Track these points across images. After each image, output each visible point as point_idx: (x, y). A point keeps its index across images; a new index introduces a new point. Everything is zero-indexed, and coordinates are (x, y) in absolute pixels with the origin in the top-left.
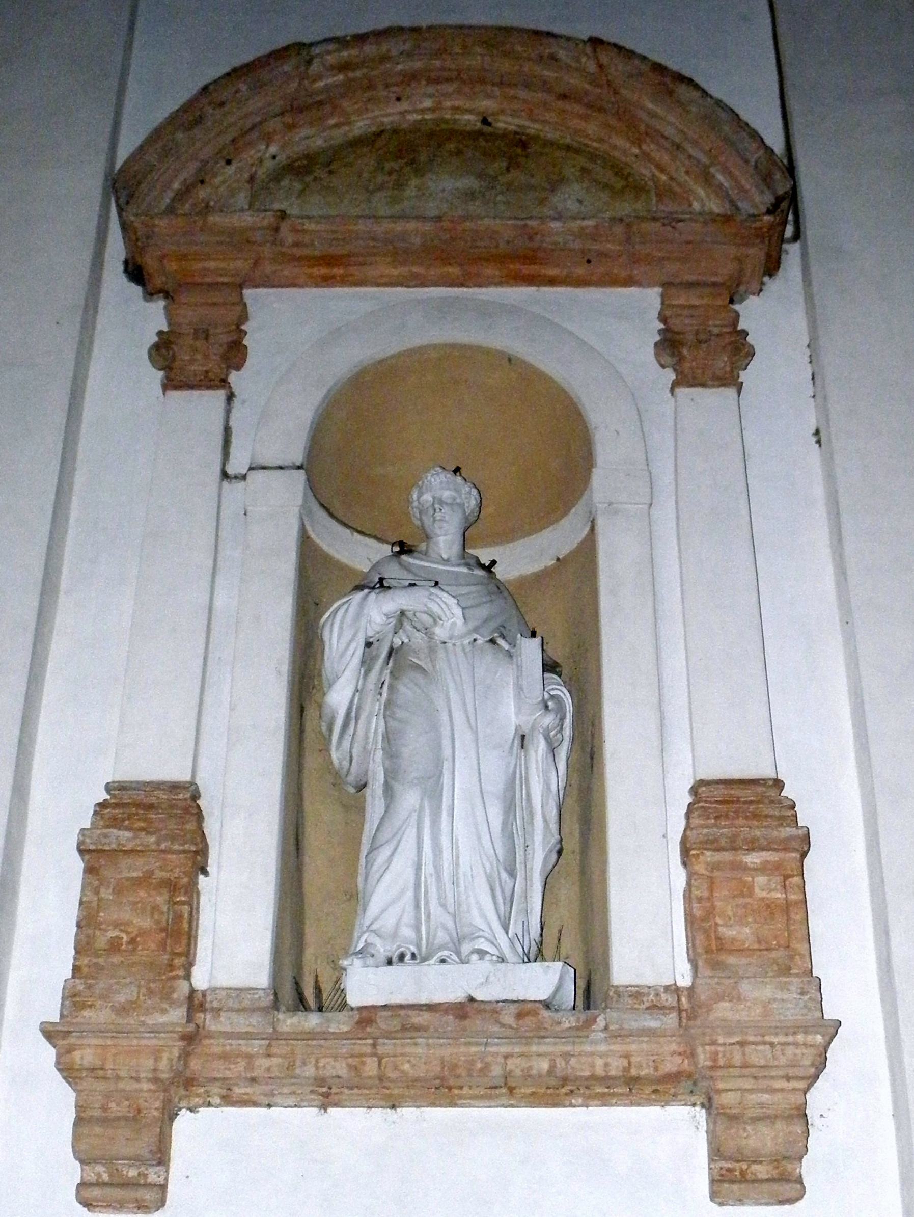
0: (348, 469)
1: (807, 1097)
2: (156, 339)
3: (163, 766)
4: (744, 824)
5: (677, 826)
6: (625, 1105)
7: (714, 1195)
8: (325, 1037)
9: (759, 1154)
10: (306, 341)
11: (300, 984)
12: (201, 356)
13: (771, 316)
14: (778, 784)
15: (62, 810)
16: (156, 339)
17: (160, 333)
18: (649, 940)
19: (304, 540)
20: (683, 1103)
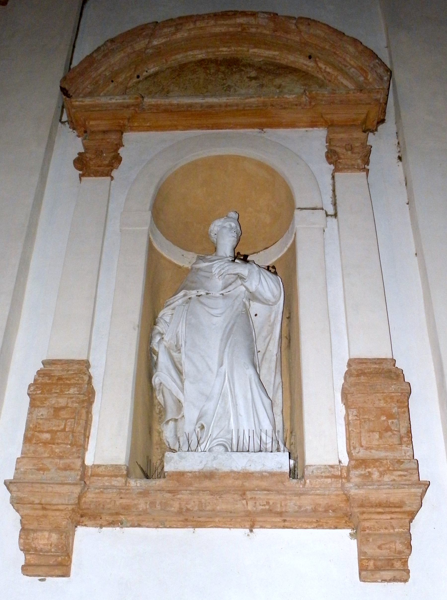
0: (176, 220)
1: (411, 524)
2: (77, 156)
3: (68, 349)
4: (377, 387)
5: (340, 382)
6: (275, 526)
7: (363, 579)
8: (157, 487)
9: (386, 560)
10: (148, 154)
11: (146, 462)
12: (98, 162)
13: (382, 144)
14: (394, 361)
15: (23, 371)
16: (77, 156)
17: (80, 154)
18: (327, 440)
19: (151, 249)
20: (315, 525)
